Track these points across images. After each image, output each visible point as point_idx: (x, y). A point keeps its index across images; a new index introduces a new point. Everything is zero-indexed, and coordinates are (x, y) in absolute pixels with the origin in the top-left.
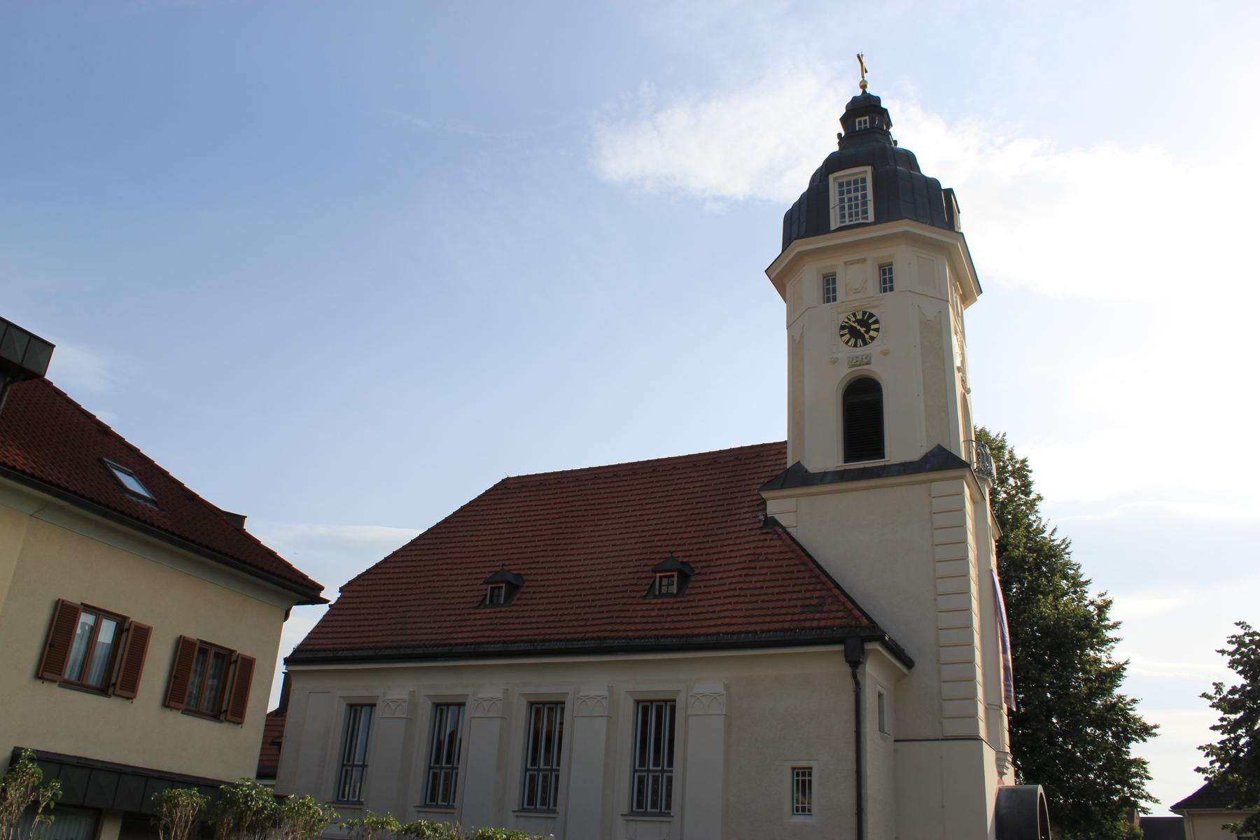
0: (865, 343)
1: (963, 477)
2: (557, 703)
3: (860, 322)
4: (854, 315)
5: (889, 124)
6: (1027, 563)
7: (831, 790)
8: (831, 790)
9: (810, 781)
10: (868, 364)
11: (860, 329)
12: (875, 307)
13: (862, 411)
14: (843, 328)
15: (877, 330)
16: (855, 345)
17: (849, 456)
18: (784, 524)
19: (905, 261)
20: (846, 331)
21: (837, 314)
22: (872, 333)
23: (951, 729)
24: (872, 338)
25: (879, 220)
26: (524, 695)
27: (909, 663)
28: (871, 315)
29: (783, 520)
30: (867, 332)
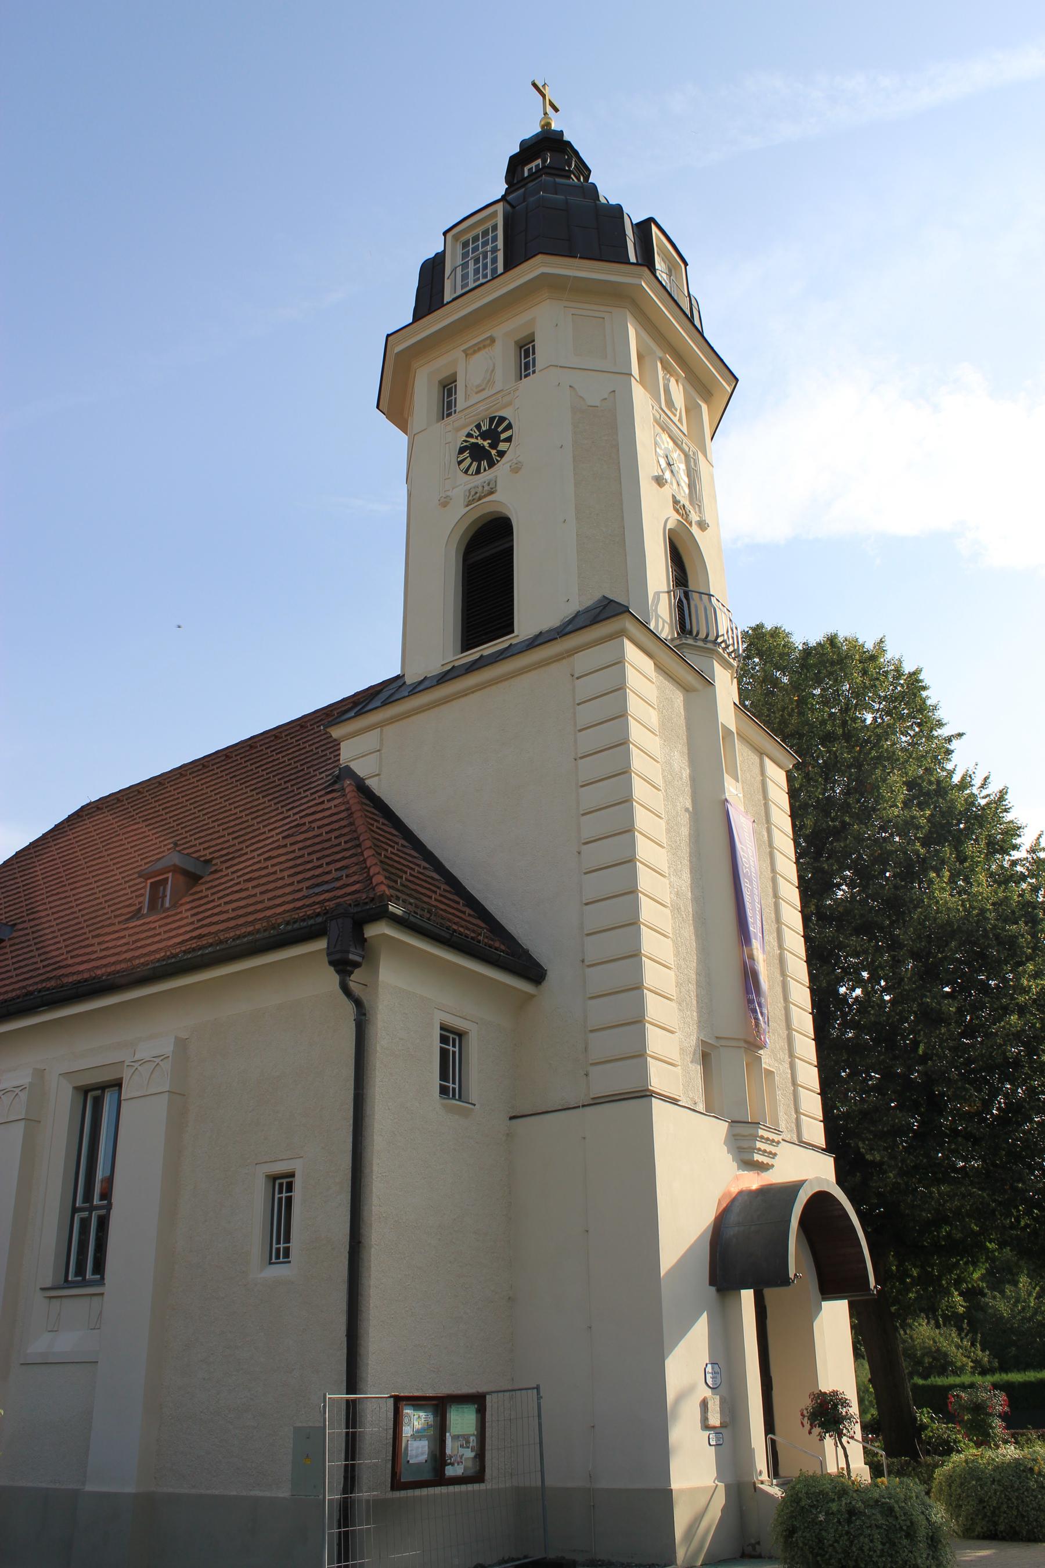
0: (492, 464)
1: (622, 633)
2: (103, 1087)
3: (484, 436)
4: (478, 427)
5: (584, 170)
6: (918, 828)
7: (319, 1215)
8: (319, 1215)
9: (289, 1200)
10: (491, 493)
11: (486, 446)
12: (505, 406)
13: (484, 575)
14: (462, 450)
15: (509, 440)
16: (478, 472)
17: (468, 642)
18: (361, 773)
19: (551, 322)
20: (466, 454)
21: (457, 431)
22: (502, 446)
23: (603, 1082)
24: (501, 454)
25: (509, 266)
26: (66, 1075)
27: (532, 972)
28: (502, 419)
29: (360, 769)
30: (493, 446)
